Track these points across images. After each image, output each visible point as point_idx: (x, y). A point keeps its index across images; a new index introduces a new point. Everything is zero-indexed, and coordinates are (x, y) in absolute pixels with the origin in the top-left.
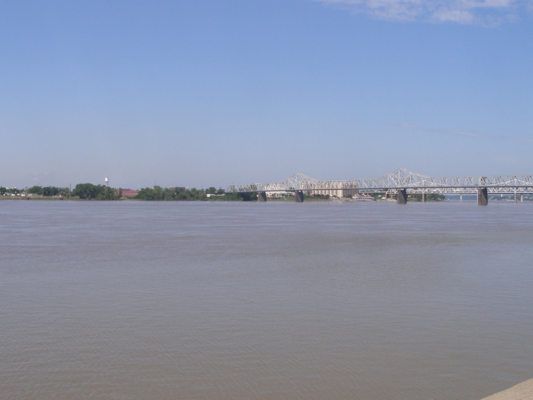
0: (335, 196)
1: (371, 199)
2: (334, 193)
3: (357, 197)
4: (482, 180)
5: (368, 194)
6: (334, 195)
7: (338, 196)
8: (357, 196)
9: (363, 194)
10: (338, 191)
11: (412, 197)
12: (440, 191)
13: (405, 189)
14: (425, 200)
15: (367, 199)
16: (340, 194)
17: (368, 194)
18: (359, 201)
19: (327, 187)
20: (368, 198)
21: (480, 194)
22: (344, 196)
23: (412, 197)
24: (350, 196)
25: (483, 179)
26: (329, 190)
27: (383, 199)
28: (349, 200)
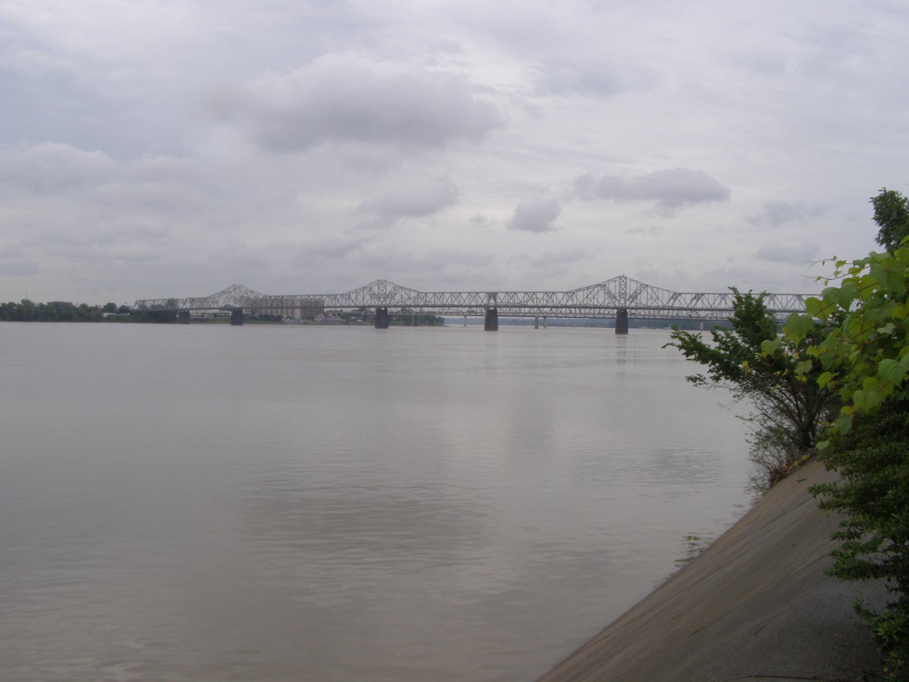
0: (290, 317)
6: (289, 315)
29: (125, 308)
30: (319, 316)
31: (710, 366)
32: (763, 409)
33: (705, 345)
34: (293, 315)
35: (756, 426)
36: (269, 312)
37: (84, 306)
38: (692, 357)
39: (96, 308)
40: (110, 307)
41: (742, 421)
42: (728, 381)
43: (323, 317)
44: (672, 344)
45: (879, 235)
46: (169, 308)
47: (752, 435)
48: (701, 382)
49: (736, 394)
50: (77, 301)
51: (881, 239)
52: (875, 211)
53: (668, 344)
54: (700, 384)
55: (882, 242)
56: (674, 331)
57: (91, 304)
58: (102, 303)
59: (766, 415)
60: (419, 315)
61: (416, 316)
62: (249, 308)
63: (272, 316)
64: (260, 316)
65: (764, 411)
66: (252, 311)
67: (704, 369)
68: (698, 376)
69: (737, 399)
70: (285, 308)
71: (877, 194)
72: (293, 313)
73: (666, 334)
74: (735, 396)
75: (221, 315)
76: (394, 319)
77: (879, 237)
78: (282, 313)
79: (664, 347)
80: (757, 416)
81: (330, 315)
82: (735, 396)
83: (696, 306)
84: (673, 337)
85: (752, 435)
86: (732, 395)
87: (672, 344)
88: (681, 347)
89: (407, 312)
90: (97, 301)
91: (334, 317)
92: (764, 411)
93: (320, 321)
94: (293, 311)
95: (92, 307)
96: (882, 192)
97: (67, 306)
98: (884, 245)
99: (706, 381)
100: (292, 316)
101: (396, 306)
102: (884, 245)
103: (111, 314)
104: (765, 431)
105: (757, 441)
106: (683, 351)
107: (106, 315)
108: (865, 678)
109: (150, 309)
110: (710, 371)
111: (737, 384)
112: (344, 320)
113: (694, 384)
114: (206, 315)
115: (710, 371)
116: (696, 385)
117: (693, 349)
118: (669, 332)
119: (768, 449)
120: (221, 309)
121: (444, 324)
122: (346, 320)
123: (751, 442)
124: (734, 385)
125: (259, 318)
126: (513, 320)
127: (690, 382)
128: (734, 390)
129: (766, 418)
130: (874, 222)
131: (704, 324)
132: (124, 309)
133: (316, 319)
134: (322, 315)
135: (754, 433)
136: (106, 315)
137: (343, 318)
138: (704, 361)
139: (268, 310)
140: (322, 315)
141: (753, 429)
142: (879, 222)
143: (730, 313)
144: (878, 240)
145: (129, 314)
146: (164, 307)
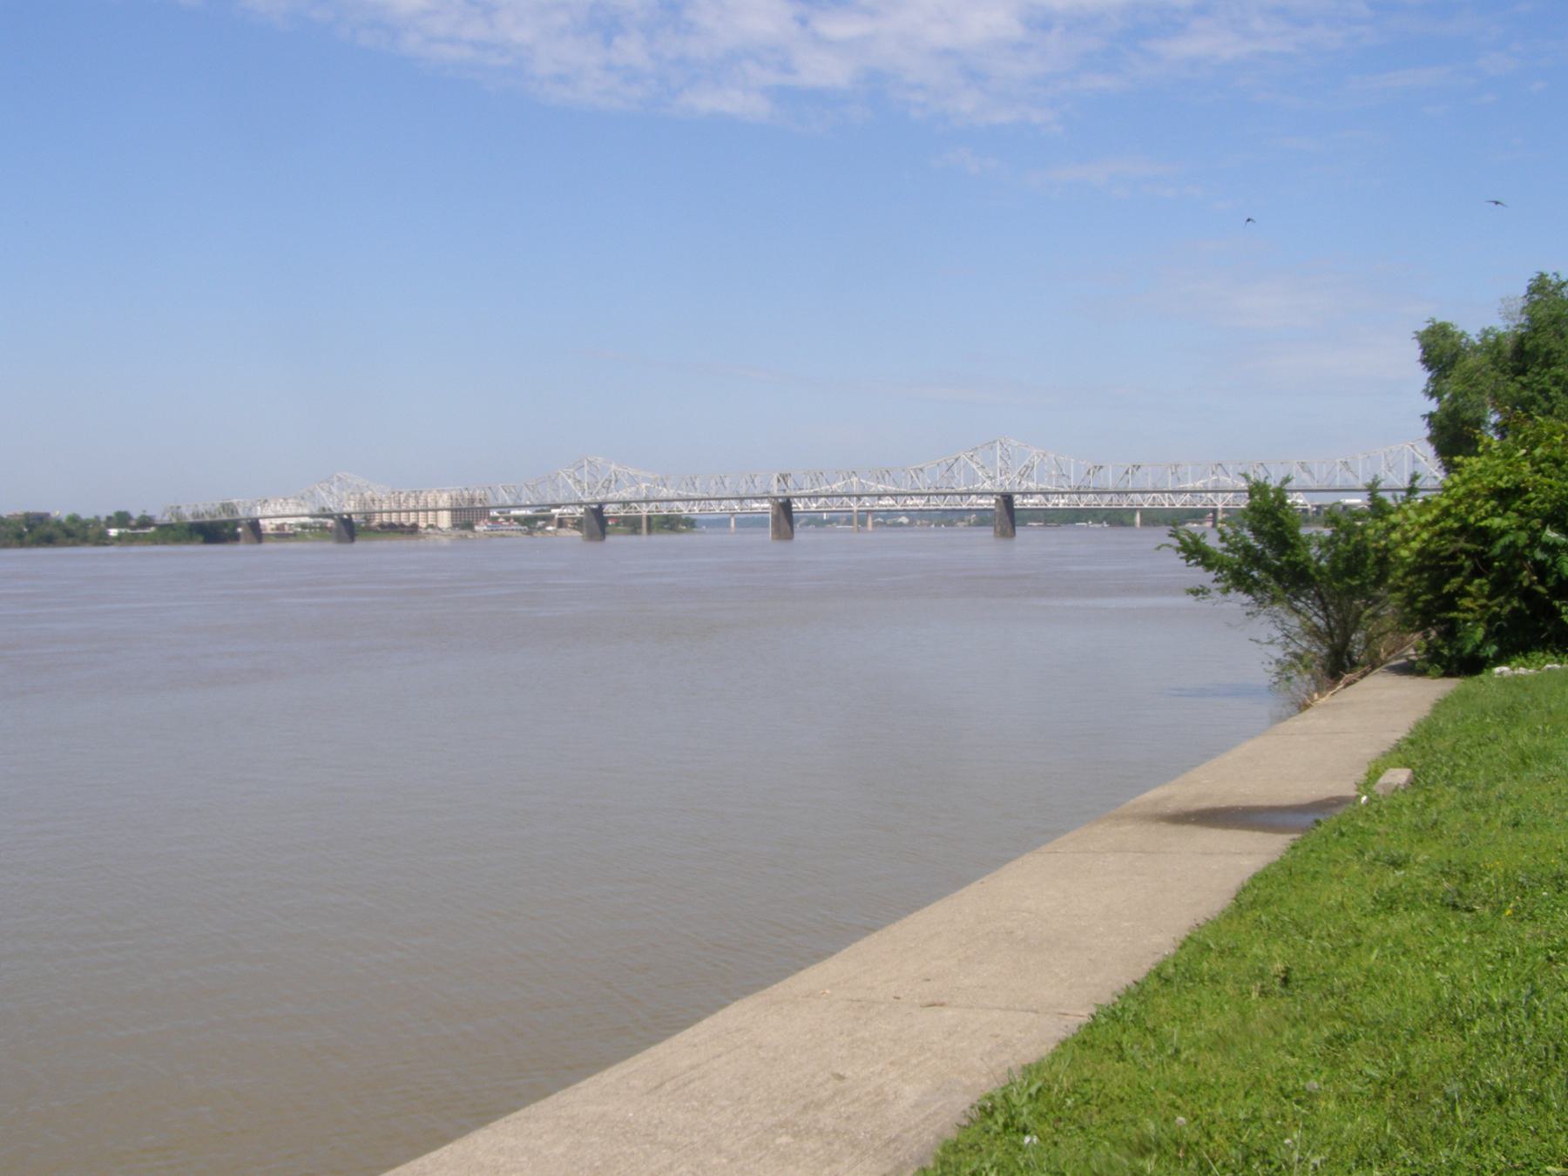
0: (431, 526)
1: (521, 530)
2: (429, 520)
3: (485, 528)
4: (779, 481)
5: (512, 520)
6: (430, 523)
7: (440, 525)
8: (486, 524)
9: (500, 520)
10: (440, 513)
11: (617, 524)
12: (683, 509)
13: (601, 505)
14: (650, 530)
15: (510, 533)
16: (445, 520)
17: (512, 520)
18: (490, 536)
19: (412, 503)
20: (513, 530)
21: (775, 513)
22: (454, 526)
23: (617, 524)
24: (469, 526)
25: (781, 479)
26: (417, 511)
27: (549, 532)
28: (466, 536)
29: (147, 519)
30: (482, 523)
31: (1216, 574)
32: (1285, 629)
33: (1215, 548)
34: (436, 521)
35: (1277, 653)
36: (394, 519)
37: (74, 519)
38: (1192, 561)
39: (97, 521)
40: (122, 519)
41: (1257, 646)
42: (1240, 594)
43: (490, 524)
44: (1170, 546)
45: (1427, 385)
46: (224, 517)
47: (1270, 663)
48: (1205, 596)
49: (1249, 611)
50: (60, 512)
51: (1430, 390)
52: (1421, 351)
53: (1163, 545)
54: (1203, 598)
55: (1432, 395)
56: (1171, 528)
57: (86, 514)
58: (106, 512)
59: (1288, 637)
60: (655, 516)
61: (649, 518)
62: (360, 513)
63: (402, 525)
64: (382, 526)
65: (1285, 632)
66: (365, 518)
67: (1201, 576)
68: (1200, 588)
69: (1251, 616)
70: (412, 511)
71: (1423, 327)
72: (436, 518)
73: (1161, 534)
74: (1248, 614)
75: (313, 525)
76: (610, 523)
77: (1428, 388)
78: (418, 519)
79: (1159, 548)
80: (1278, 638)
81: (500, 520)
82: (1248, 614)
83: (1424, 483)
84: (1170, 536)
85: (1270, 663)
86: (1244, 612)
87: (1170, 546)
88: (1178, 550)
89: (632, 510)
90: (92, 508)
91: (507, 523)
92: (1285, 632)
93: (485, 530)
94: (436, 515)
95: (87, 520)
96: (1431, 324)
97: (42, 518)
98: (1435, 400)
99: (1210, 594)
100: (434, 523)
101: (982, 494)
102: (1435, 400)
103: (123, 530)
104: (1288, 658)
105: (1278, 670)
106: (1182, 554)
107: (113, 532)
108: (1565, 990)
109: (191, 520)
110: (1216, 580)
111: (1250, 597)
112: (526, 527)
113: (1195, 598)
114: (286, 527)
115: (1216, 580)
116: (1198, 600)
117: (1195, 552)
118: (1166, 530)
119: (1273, 674)
120: (312, 516)
121: (695, 529)
122: (529, 528)
123: (1270, 672)
124: (1247, 599)
125: (379, 529)
126: (747, 519)
127: (1191, 596)
128: (1247, 604)
129: (1288, 640)
130: (1420, 366)
131: (1141, 515)
132: (145, 522)
133: (477, 528)
134: (486, 520)
135: (1273, 662)
136: (113, 532)
137: (523, 524)
138: (1209, 567)
139: (384, 514)
140: (486, 520)
141: (1271, 657)
142: (1427, 366)
143: (872, 506)
144: (1426, 391)
145: (152, 529)
146: (215, 516)
